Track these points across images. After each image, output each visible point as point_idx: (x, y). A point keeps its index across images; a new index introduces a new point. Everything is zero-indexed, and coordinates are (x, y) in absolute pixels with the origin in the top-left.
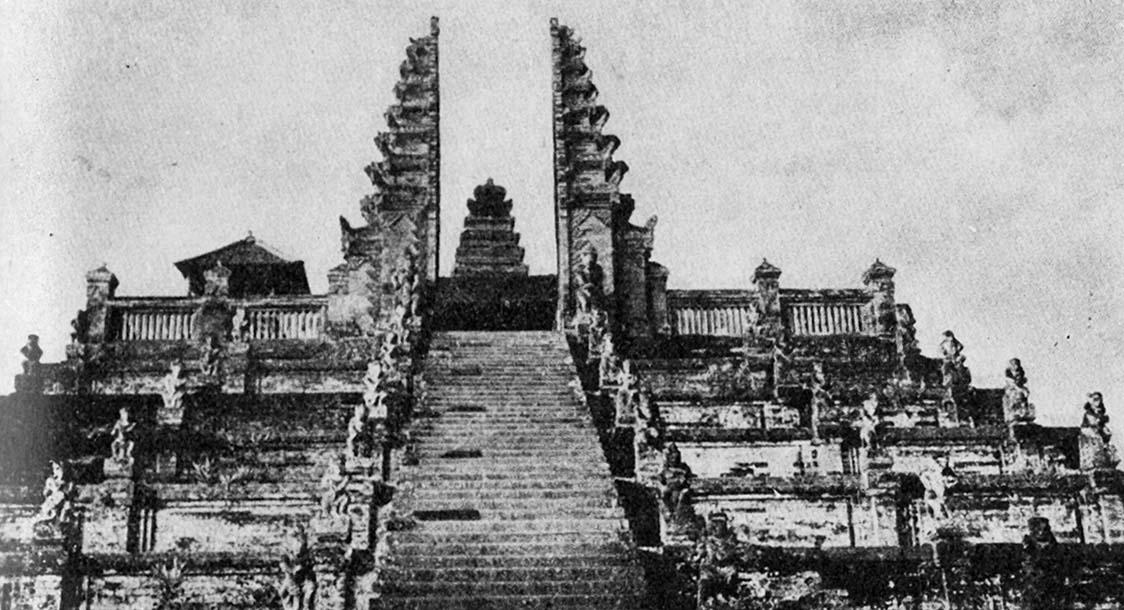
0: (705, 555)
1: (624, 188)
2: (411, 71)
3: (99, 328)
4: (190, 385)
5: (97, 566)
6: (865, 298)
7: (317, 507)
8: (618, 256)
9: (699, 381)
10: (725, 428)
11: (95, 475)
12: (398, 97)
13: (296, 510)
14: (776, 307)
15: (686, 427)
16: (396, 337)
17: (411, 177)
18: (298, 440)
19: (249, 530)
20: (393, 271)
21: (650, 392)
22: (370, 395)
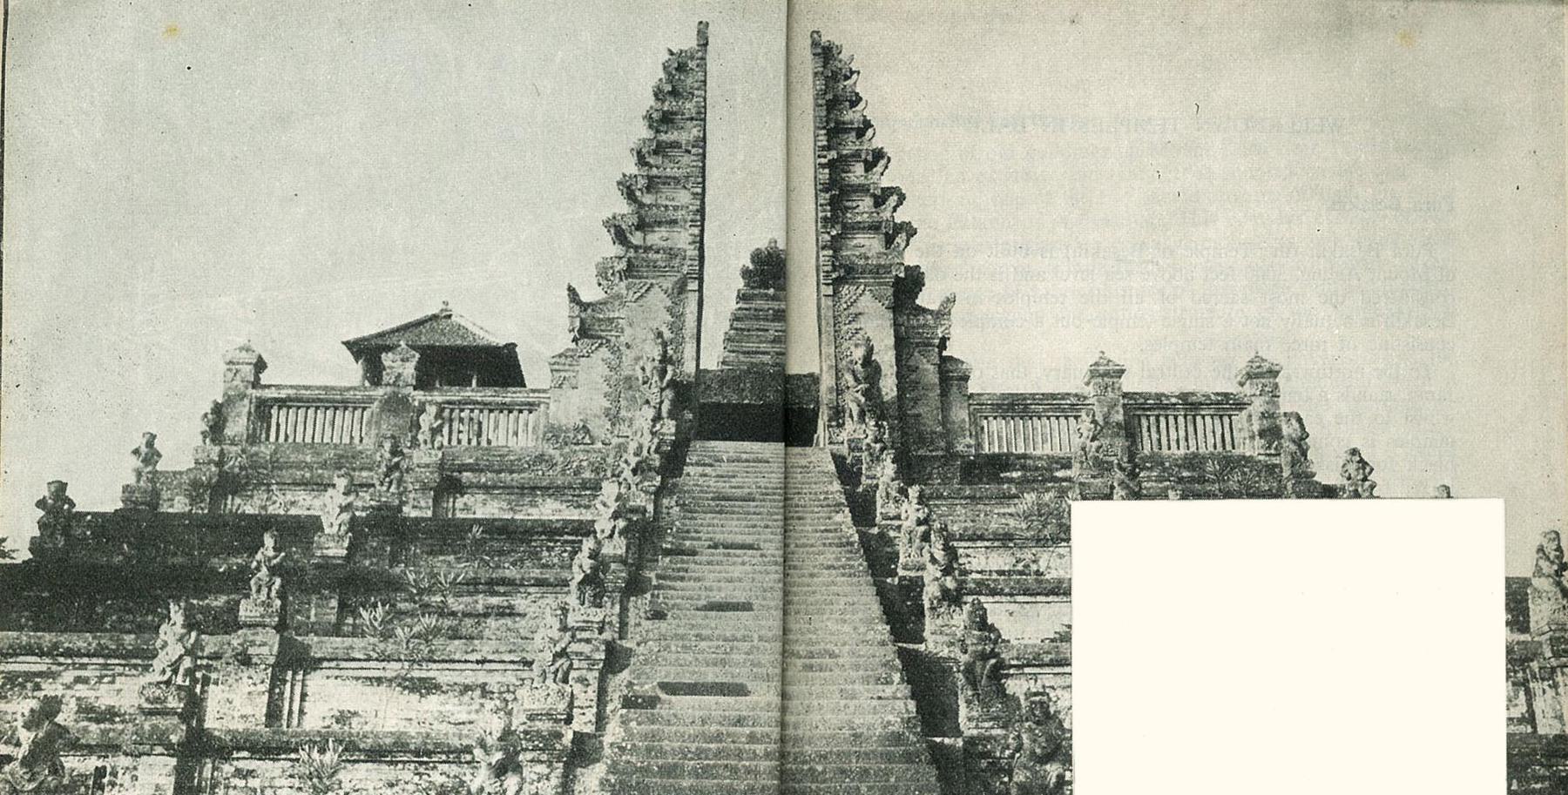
0: (1019, 748)
1: (910, 259)
2: (670, 93)
3: (237, 426)
4: (359, 504)
5: (222, 750)
6: (1240, 405)
7: (525, 675)
8: (902, 344)
9: (1011, 515)
10: (1048, 577)
11: (227, 622)
12: (650, 127)
13: (498, 677)
14: (1119, 417)
15: (995, 576)
16: (640, 447)
17: (666, 235)
18: (503, 581)
19: (433, 702)
20: (638, 359)
21: (945, 529)
22: (603, 524)
